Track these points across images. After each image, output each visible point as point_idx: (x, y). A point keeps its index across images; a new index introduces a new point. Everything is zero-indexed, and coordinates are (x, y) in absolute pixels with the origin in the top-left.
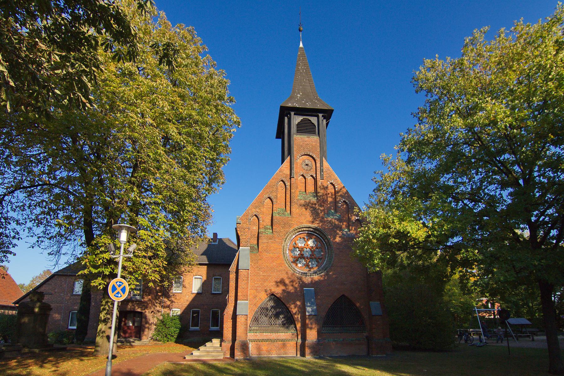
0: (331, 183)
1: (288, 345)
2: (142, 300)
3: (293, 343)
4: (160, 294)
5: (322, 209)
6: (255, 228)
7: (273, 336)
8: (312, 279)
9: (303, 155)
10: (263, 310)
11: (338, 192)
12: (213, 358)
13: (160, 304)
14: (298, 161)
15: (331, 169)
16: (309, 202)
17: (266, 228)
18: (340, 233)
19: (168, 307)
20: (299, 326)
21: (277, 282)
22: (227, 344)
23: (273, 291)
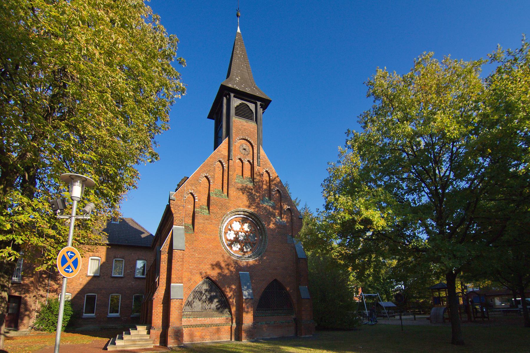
0: (267, 171)
1: (223, 330)
2: (22, 282)
3: (228, 327)
4: (44, 276)
5: (258, 194)
6: (191, 207)
7: (207, 321)
8: (247, 263)
9: (241, 139)
10: (198, 294)
11: (273, 181)
12: (142, 348)
13: (44, 287)
14: (236, 144)
15: (267, 157)
16: (246, 187)
17: (202, 208)
18: (274, 220)
19: (55, 291)
20: (234, 309)
21: (212, 265)
22: (157, 332)
23: (208, 273)
